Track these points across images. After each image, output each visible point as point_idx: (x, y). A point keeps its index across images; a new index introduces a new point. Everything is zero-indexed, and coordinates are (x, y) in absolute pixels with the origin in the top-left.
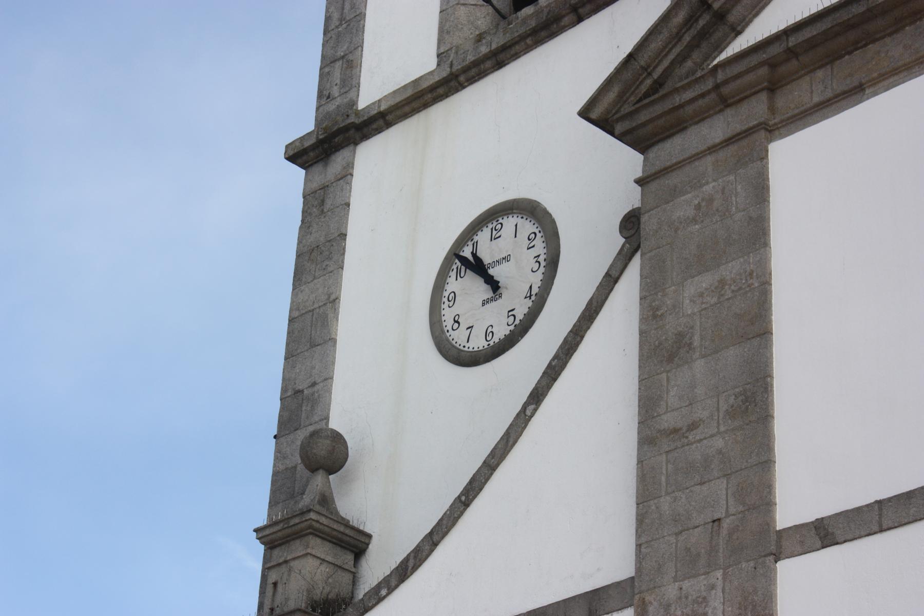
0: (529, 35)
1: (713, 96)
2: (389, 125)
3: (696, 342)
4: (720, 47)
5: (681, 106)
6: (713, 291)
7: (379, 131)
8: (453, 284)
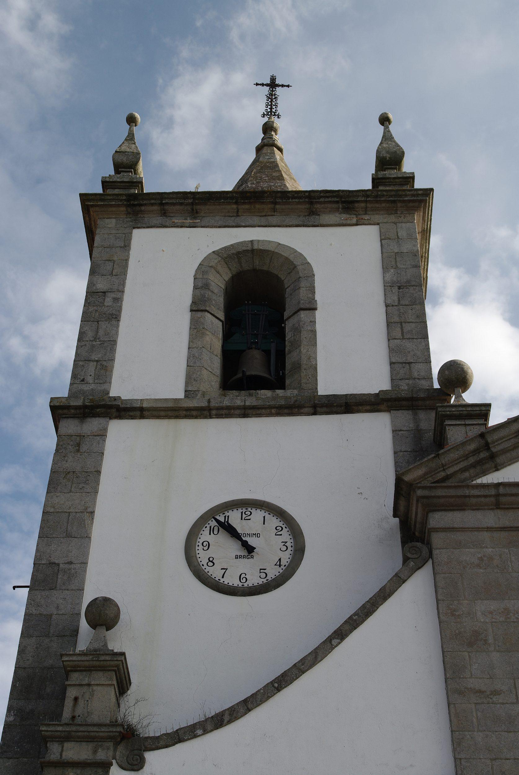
0: (277, 408)
1: (493, 499)
2: (142, 417)
3: (491, 640)
4: (485, 473)
5: (469, 497)
6: (500, 613)
7: (133, 418)
8: (205, 536)
